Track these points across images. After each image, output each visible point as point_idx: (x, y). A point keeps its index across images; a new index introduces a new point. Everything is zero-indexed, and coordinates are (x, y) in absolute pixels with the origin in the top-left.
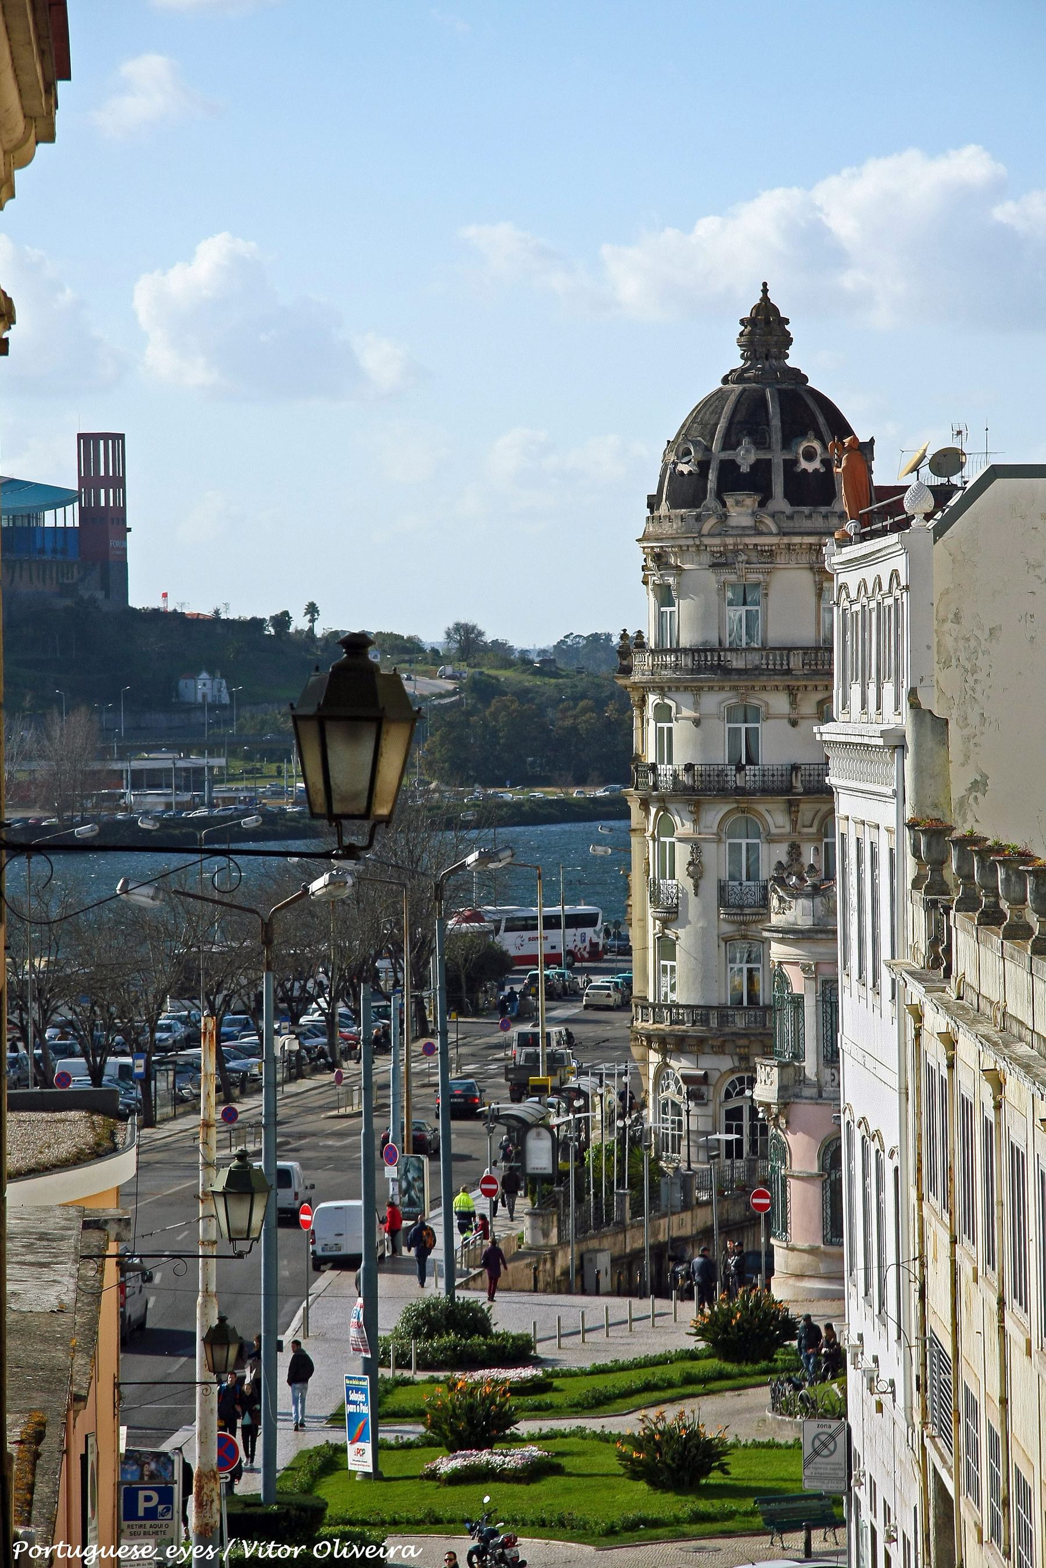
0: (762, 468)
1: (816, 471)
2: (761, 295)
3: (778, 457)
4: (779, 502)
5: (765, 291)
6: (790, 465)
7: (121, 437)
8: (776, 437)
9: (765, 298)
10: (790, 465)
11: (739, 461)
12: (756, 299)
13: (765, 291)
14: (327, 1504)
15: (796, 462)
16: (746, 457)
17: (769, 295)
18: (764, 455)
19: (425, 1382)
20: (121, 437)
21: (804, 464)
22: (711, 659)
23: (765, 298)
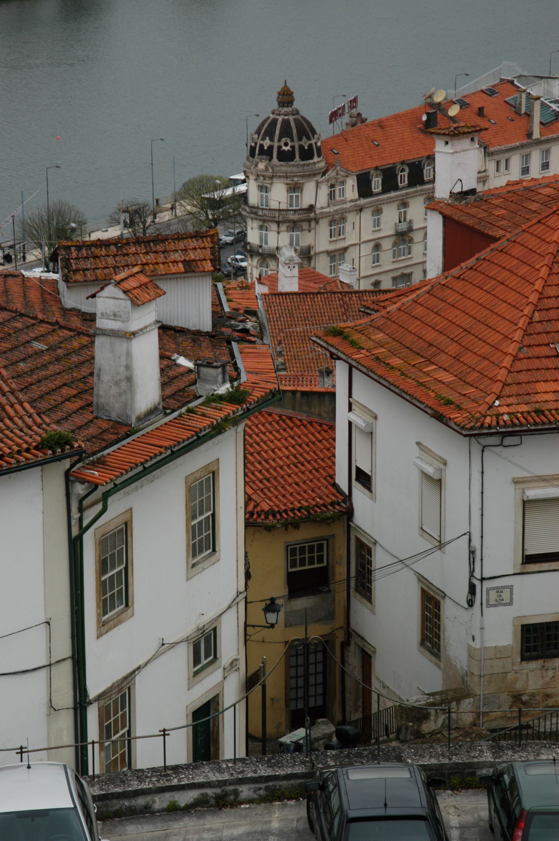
0: (271, 148)
1: (288, 150)
2: (284, 84)
3: (276, 145)
4: (275, 160)
5: (286, 83)
6: (279, 147)
7: (512, 604)
8: (295, 138)
9: (286, 86)
10: (279, 147)
11: (264, 145)
12: (282, 85)
13: (286, 83)
14: (263, 610)
15: (281, 147)
16: (267, 143)
17: (287, 84)
18: (262, 142)
19: (107, 420)
20: (512, 604)
21: (284, 148)
22: (254, 210)
23: (286, 86)
